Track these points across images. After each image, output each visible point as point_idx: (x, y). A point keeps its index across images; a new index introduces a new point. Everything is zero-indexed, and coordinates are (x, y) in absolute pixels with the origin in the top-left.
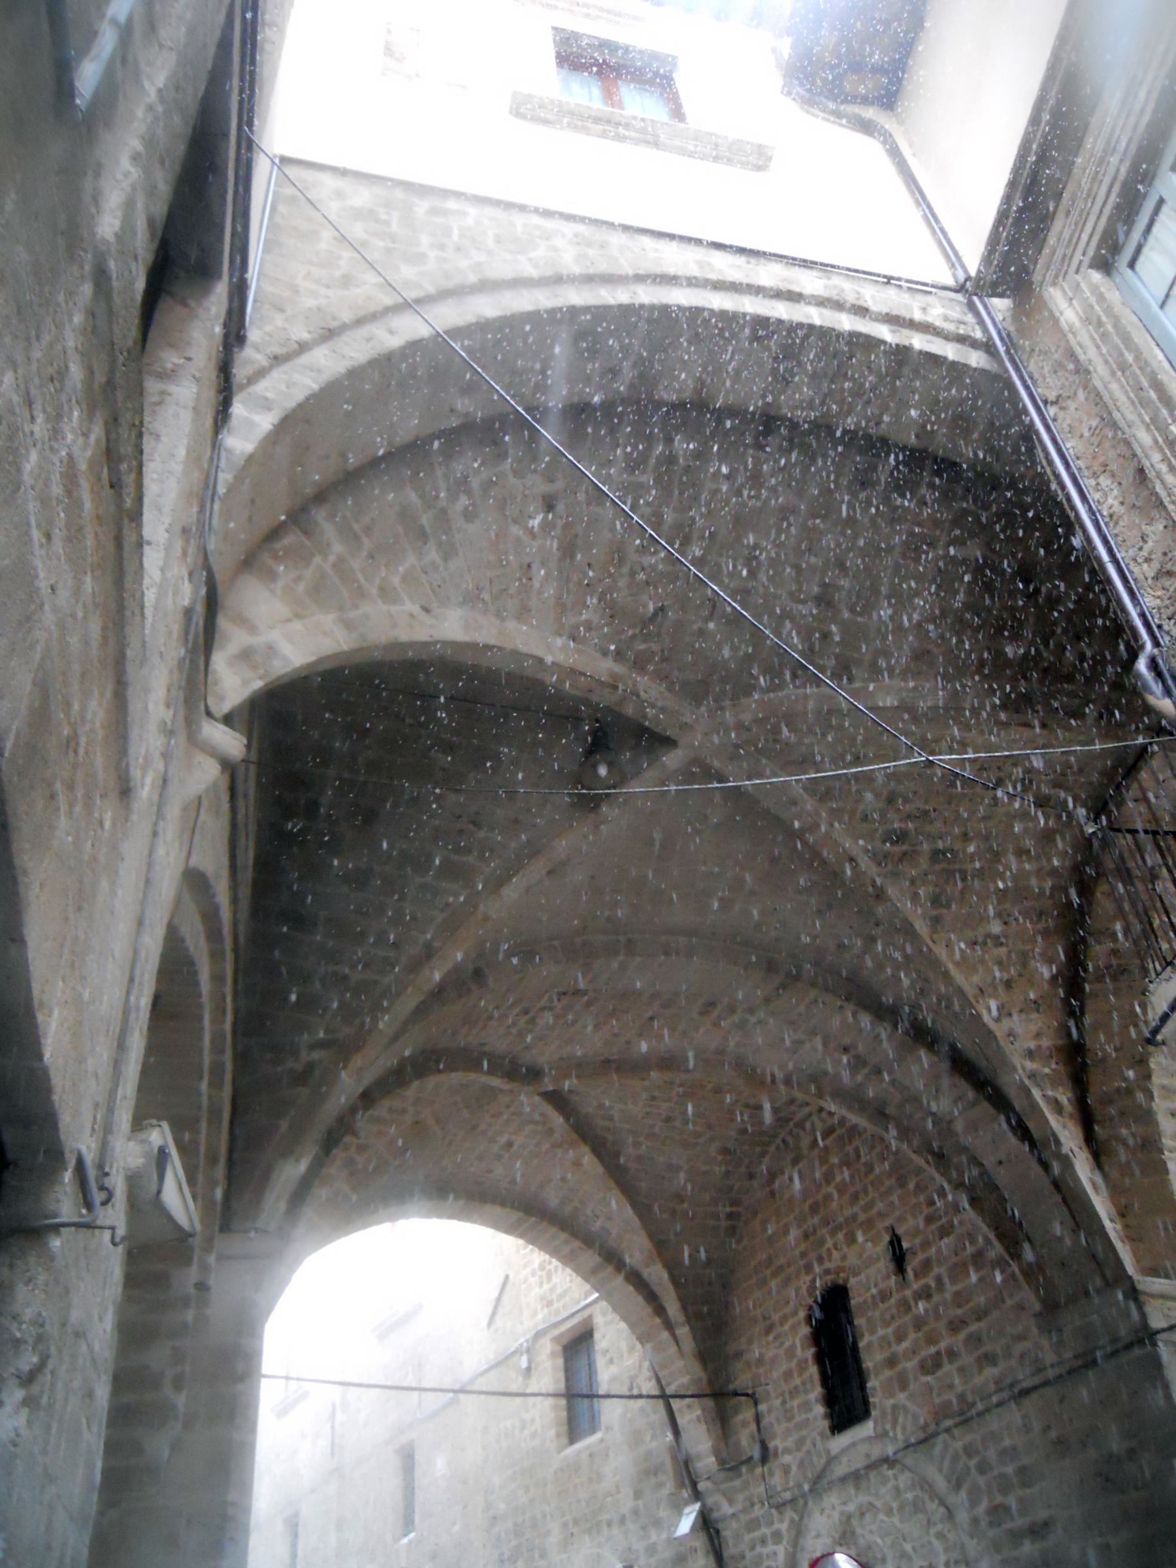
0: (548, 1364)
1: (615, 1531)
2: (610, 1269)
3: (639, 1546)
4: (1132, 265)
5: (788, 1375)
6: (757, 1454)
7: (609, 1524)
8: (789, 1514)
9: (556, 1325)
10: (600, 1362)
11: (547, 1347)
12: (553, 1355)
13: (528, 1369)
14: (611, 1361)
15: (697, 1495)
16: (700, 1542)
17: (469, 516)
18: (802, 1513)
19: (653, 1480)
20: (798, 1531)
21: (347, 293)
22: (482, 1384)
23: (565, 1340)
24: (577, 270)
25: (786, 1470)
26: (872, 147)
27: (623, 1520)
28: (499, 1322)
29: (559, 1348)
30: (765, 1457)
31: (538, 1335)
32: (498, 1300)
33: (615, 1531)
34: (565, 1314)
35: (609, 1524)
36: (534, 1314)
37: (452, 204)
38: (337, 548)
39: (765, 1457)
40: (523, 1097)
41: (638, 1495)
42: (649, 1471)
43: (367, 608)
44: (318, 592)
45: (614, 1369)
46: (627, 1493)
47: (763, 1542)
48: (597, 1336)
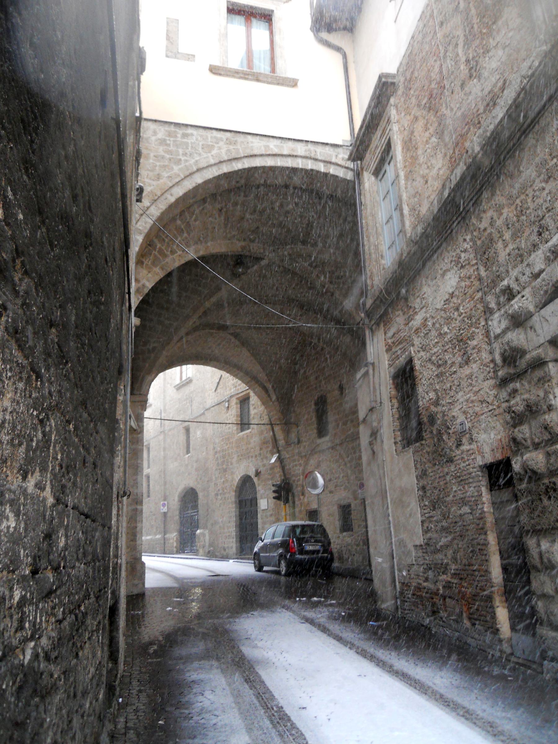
0: (235, 406)
1: (253, 459)
2: (253, 382)
3: (260, 464)
4: (389, 164)
5: (307, 420)
6: (296, 440)
7: (252, 457)
8: (304, 459)
9: (238, 394)
10: (251, 408)
11: (234, 401)
12: (236, 404)
13: (228, 407)
14: (255, 408)
15: (279, 452)
16: (278, 464)
17: (195, 220)
18: (308, 460)
19: (266, 445)
20: (306, 464)
21: (159, 182)
22: (209, 417)
23: (241, 399)
24: (226, 158)
25: (305, 447)
26: (336, 59)
27: (256, 456)
28: (219, 390)
29: (238, 401)
30: (299, 442)
31: (231, 397)
32: (218, 383)
33: (253, 459)
34: (240, 391)
35: (252, 457)
36: (231, 389)
37: (190, 131)
38: (159, 245)
39: (299, 442)
40: (175, 534)
41: (261, 449)
42: (264, 443)
43: (168, 260)
44: (154, 264)
45: (256, 411)
46: (258, 448)
47: (296, 465)
48: (251, 399)
